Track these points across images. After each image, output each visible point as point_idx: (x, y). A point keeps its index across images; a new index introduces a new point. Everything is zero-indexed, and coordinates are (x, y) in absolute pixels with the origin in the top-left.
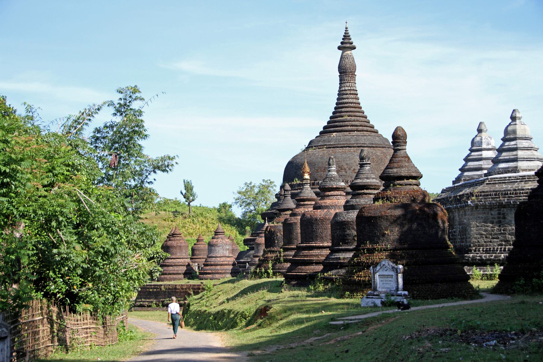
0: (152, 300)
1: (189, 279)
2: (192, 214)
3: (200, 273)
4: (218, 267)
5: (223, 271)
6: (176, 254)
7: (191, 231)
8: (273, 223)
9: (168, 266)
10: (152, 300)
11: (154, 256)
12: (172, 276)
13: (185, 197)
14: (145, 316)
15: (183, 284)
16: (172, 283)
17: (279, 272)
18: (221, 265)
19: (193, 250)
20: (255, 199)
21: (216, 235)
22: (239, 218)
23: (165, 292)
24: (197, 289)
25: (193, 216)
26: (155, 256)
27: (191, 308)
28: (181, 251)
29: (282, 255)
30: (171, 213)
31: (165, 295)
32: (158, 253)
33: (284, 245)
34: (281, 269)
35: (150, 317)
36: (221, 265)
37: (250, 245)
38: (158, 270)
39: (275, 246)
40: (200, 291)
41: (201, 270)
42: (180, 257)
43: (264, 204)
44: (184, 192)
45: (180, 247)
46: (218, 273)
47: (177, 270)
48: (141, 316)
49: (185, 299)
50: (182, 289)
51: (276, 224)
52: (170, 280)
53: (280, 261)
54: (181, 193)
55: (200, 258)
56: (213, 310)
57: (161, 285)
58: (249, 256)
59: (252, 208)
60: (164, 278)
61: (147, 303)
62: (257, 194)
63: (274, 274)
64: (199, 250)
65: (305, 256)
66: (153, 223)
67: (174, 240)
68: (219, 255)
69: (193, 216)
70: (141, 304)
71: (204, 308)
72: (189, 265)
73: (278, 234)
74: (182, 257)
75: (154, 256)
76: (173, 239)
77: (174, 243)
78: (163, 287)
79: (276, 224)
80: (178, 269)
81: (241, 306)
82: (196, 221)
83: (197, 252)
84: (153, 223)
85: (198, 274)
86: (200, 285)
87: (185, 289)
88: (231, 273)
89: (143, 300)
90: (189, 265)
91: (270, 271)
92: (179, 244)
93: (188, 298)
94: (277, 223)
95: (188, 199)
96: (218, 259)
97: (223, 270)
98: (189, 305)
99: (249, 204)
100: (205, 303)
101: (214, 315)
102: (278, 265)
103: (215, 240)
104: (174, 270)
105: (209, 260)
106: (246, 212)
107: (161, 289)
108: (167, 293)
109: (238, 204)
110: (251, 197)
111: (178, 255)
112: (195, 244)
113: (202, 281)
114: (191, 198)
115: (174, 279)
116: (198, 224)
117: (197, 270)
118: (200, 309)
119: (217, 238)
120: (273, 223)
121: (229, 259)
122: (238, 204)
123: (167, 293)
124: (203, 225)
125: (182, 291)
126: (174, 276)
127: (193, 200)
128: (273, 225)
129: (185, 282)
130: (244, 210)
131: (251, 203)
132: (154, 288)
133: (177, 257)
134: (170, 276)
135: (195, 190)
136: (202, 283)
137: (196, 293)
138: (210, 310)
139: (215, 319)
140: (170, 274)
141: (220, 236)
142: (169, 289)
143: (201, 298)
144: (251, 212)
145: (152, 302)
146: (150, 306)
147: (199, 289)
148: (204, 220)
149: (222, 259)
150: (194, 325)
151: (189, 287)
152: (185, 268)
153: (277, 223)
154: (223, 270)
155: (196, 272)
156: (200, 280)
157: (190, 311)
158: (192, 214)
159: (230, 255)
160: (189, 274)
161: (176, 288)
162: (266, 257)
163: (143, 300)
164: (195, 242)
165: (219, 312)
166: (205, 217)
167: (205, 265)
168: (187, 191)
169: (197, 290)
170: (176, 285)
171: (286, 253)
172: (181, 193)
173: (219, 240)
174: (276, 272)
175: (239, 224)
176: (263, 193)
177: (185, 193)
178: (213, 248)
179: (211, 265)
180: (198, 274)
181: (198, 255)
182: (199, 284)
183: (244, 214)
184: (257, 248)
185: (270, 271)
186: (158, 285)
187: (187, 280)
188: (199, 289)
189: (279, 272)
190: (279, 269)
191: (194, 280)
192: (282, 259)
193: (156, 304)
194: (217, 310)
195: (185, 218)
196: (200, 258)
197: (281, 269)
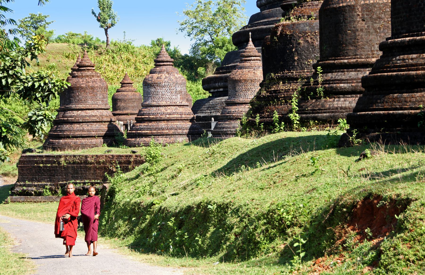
0: (43, 183)
1: (109, 145)
2: (112, 47)
3: (130, 135)
4: (163, 124)
5: (172, 132)
6: (85, 101)
7: (111, 75)
8: (289, 19)
9: (72, 123)
10: (43, 183)
11: (33, 85)
12: (79, 141)
13: (99, 20)
14: (30, 211)
15: (99, 154)
16: (79, 152)
17: (314, 119)
18: (168, 120)
19: (115, 100)
20: (211, 23)
21: (156, 66)
22: (186, 56)
23: (66, 168)
24: (125, 163)
25: (113, 51)
26: (37, 84)
27: (118, 197)
28: (95, 95)
29: (320, 80)
30: (77, 46)
31: (67, 174)
32: (42, 78)
33: (323, 57)
34: (320, 111)
35: (39, 214)
36: (168, 120)
37: (215, 88)
38: (45, 116)
39: (294, 68)
40: (130, 167)
41: (132, 129)
42: (93, 107)
43: (226, 30)
44: (98, 11)
45: (93, 88)
46: (162, 135)
47: (88, 131)
48: (23, 212)
49: (105, 180)
50: (99, 163)
51: (295, 21)
52: (76, 147)
53: (315, 93)
54: (93, 13)
55: (127, 114)
56: (173, 203)
57: (60, 156)
58: (213, 107)
59: (207, 37)
60: (66, 144)
61: (34, 189)
62: (215, 15)
63: (304, 123)
64: (125, 101)
65: (410, 67)
66: (48, 61)
67: (82, 77)
68: (164, 103)
69: (113, 51)
70: (24, 191)
71: (146, 200)
72: (111, 121)
73: (301, 41)
74: (96, 107)
75: (33, 85)
76: (79, 74)
77: (82, 82)
78: (62, 159)
79: (295, 21)
80: (89, 128)
81: (256, 195)
82: (117, 59)
83: (121, 104)
84: (48, 61)
85: (125, 136)
86: (130, 156)
87: (103, 163)
88: (188, 135)
89: (27, 183)
90: (111, 121)
91: (295, 117)
92: (91, 84)
93: (109, 178)
94: (298, 18)
95: (104, 22)
96: (163, 109)
97: (171, 129)
98: (112, 193)
99: (203, 32)
100: (148, 188)
101: (176, 215)
102: (311, 103)
103: (155, 76)
104: (83, 130)
105: (146, 111)
106: (199, 44)
107: (59, 163)
108: (70, 170)
109: (185, 32)
110: (206, 19)
111: (90, 104)
112: (118, 91)
113: (134, 149)
114: (109, 22)
115: (84, 146)
116: (121, 63)
117: (122, 129)
118: (138, 200)
119: (160, 72)
120: (289, 19)
121: (181, 110)
122: (185, 32)
123: (70, 170)
124: (130, 66)
125: (98, 166)
126: (84, 141)
127: (112, 25)
128: (288, 22)
129: (102, 150)
130: (194, 41)
131: (206, 30)
132: (47, 162)
133: (88, 106)
134: (75, 140)
135: (114, 11)
136: (134, 152)
137: (126, 170)
138: (164, 205)
139: (180, 225)
140: (76, 137)
141: (164, 68)
142: (74, 163)
143: (137, 177)
144: (205, 44)
145: (43, 187)
146: (40, 194)
147: (129, 163)
148: (131, 57)
149: (170, 110)
150: (126, 234)
151: (111, 159)
152: (104, 127)
153: (298, 18)
154: (171, 129)
155: (122, 134)
156: (130, 146)
157: (115, 203)
158: (112, 47)
159: (184, 103)
160: (112, 137)
161: (86, 162)
162: (275, 91)
163: (27, 183)
164: (119, 86)
165: (189, 208)
166: (132, 53)
167: (139, 120)
168: (103, 10)
169: (126, 164)
170: (86, 157)
171: (330, 76)
172: (93, 13)
173: (164, 75)
174: (308, 119)
175: (189, 65)
176: (225, 13)
177: (100, 14)
178: (153, 90)
179: (150, 121)
180: (125, 136)
181: (124, 108)
182: (129, 154)
183: (195, 49)
184: (234, 88)
185: (295, 117)
186: (53, 157)
187: (106, 148)
188: (129, 163)
189: (314, 119)
190: (313, 111)
191: (118, 147)
192: (320, 89)
193: (51, 190)
194: (184, 204)
195: (101, 54)
196: (127, 114)
197: (320, 111)
